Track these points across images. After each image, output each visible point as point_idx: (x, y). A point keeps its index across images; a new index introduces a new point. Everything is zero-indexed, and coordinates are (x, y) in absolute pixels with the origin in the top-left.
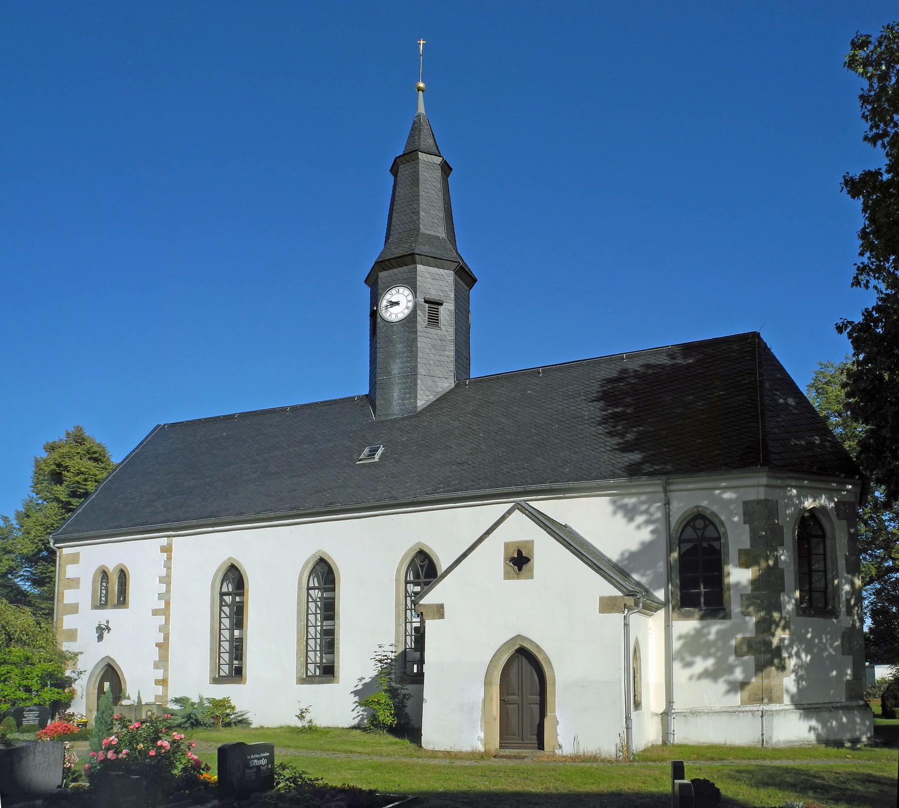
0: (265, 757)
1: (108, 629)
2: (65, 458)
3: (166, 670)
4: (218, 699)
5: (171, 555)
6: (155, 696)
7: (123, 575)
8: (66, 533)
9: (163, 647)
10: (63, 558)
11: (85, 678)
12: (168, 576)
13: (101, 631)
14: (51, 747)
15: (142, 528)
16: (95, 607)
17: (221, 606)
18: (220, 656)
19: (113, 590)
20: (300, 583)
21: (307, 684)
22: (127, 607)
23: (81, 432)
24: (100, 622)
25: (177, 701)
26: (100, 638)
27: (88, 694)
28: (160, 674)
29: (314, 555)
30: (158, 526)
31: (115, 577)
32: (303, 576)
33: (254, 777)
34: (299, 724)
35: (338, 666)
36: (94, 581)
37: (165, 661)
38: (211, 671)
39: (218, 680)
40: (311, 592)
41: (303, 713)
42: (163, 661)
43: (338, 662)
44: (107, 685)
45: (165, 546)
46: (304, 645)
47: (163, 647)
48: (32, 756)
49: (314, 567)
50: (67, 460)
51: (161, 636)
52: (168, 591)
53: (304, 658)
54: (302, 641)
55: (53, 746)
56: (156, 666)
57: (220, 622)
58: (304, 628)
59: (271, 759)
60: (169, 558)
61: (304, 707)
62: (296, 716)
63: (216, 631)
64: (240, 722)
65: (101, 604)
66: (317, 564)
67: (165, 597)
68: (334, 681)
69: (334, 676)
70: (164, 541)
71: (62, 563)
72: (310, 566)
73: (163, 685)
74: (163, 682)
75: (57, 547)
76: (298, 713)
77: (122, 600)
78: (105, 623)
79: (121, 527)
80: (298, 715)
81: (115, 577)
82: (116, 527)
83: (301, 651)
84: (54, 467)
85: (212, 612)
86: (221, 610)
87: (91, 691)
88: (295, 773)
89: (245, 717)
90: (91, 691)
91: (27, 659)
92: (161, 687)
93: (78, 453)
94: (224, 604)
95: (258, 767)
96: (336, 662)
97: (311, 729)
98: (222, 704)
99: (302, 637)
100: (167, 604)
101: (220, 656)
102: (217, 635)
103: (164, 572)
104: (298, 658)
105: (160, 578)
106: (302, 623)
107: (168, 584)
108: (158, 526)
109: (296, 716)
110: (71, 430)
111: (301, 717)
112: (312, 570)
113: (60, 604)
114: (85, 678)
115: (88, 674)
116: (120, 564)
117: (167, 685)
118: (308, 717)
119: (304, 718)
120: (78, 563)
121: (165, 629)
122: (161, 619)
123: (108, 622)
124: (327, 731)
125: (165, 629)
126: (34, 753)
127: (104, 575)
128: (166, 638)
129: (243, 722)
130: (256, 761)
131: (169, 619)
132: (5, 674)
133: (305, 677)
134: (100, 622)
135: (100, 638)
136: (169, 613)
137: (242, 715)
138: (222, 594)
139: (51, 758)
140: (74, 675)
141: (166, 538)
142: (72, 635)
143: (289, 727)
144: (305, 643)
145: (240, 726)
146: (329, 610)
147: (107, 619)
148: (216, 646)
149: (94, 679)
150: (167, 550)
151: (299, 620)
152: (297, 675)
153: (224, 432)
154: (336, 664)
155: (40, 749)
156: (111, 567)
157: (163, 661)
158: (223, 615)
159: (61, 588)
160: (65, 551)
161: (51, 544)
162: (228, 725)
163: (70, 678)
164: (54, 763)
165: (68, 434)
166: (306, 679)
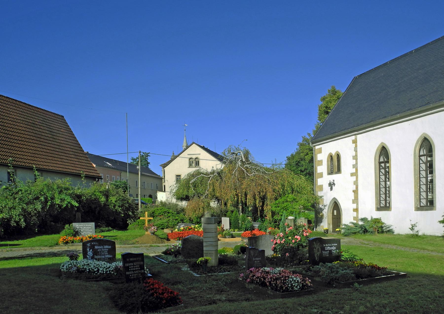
0: (335, 246)
1: (334, 184)
2: (328, 103)
3: (357, 204)
4: (369, 219)
5: (357, 145)
6: (354, 217)
7: (338, 156)
8: (316, 139)
9: (356, 192)
10: (316, 151)
11: (327, 208)
12: (356, 155)
13: (331, 185)
14: (268, 237)
15: (343, 132)
16: (329, 174)
17: (380, 169)
18: (380, 196)
19: (335, 165)
20: (415, 153)
21: (420, 211)
22: (341, 173)
23: (334, 89)
24: (330, 181)
25: (362, 220)
26: (331, 189)
27: (328, 216)
28: (355, 206)
29: (421, 136)
30: (350, 130)
31: (335, 158)
32: (416, 149)
33: (328, 255)
34: (411, 232)
35: (435, 200)
36: (328, 161)
37: (357, 199)
38: (376, 204)
39: (379, 209)
40: (422, 158)
41: (413, 227)
42: (356, 200)
43: (435, 198)
44: (335, 211)
45: (354, 140)
46: (418, 188)
47: (356, 192)
48: (261, 241)
49: (422, 143)
50: (329, 104)
51: (355, 186)
52: (357, 163)
53: (418, 196)
54: (417, 186)
55: (269, 237)
56: (353, 202)
57: (380, 178)
58: (418, 179)
59: (338, 247)
60: (356, 146)
61: (413, 223)
62: (409, 228)
63: (378, 183)
64: (389, 231)
65: (331, 173)
66: (423, 142)
67: (355, 166)
68: (433, 209)
69: (433, 206)
70: (353, 138)
71: (316, 153)
72: (420, 143)
73: (356, 212)
74: (356, 210)
75: (313, 146)
76: (411, 227)
77: (339, 171)
78: (333, 181)
79: (336, 132)
80: (410, 228)
81: (335, 158)
82: (334, 133)
83: (416, 192)
84: (325, 108)
85: (375, 173)
86: (380, 171)
87: (329, 214)
88: (351, 255)
89: (391, 228)
90: (329, 214)
91: (294, 199)
92: (356, 213)
93: (334, 99)
94: (381, 168)
95: (330, 251)
96: (434, 198)
97: (416, 236)
98: (377, 221)
99: (417, 184)
100: (357, 170)
101: (380, 196)
102: (378, 185)
103: (354, 153)
104: (415, 196)
105: (353, 156)
106: (417, 176)
107: (356, 160)
108: (350, 130)
109: (409, 228)
110: (330, 88)
111: (412, 229)
112: (421, 145)
113: (316, 173)
114: (327, 208)
115: (328, 206)
116: (337, 151)
117: (358, 212)
118: (416, 229)
119: (414, 229)
120: (321, 153)
121: (356, 183)
122: (354, 178)
123: (334, 181)
124: (424, 237)
125: (356, 183)
126: (261, 240)
127: (331, 157)
128: (357, 188)
129: (390, 231)
130: (329, 247)
131: (358, 178)
132: (285, 207)
133: (419, 206)
134: (330, 181)
135: (331, 189)
136: (358, 175)
137: (389, 227)
138: (380, 163)
139: (269, 242)
140: (323, 207)
141: (354, 136)
142: (321, 188)
143: (407, 235)
144: (419, 187)
145: (388, 233)
146: (430, 168)
147: (212, 166)
148: (378, 191)
149: (330, 209)
150: (355, 142)
151: (415, 175)
152: (415, 206)
153: (382, 73)
154: (434, 199)
155: (264, 238)
156: (334, 153)
157: (356, 200)
158: (381, 174)
159: (316, 166)
160: (317, 147)
161: (311, 145)
162: (383, 232)
163: (322, 208)
164: (270, 245)
165: (329, 91)
166: (419, 208)
